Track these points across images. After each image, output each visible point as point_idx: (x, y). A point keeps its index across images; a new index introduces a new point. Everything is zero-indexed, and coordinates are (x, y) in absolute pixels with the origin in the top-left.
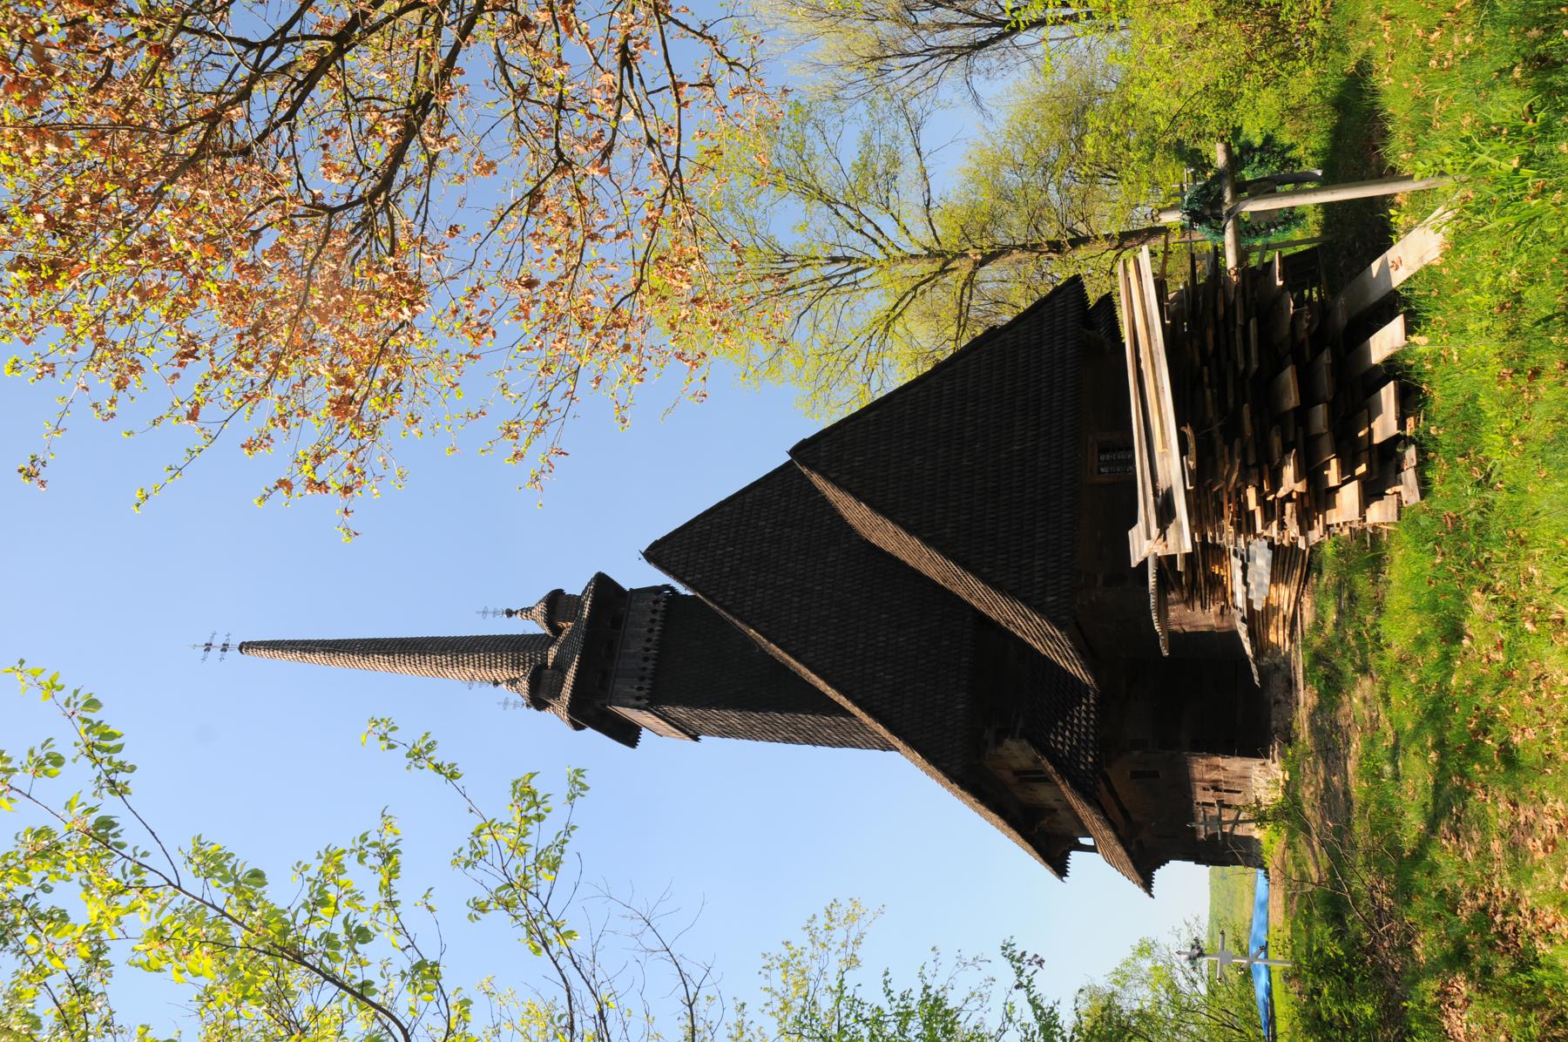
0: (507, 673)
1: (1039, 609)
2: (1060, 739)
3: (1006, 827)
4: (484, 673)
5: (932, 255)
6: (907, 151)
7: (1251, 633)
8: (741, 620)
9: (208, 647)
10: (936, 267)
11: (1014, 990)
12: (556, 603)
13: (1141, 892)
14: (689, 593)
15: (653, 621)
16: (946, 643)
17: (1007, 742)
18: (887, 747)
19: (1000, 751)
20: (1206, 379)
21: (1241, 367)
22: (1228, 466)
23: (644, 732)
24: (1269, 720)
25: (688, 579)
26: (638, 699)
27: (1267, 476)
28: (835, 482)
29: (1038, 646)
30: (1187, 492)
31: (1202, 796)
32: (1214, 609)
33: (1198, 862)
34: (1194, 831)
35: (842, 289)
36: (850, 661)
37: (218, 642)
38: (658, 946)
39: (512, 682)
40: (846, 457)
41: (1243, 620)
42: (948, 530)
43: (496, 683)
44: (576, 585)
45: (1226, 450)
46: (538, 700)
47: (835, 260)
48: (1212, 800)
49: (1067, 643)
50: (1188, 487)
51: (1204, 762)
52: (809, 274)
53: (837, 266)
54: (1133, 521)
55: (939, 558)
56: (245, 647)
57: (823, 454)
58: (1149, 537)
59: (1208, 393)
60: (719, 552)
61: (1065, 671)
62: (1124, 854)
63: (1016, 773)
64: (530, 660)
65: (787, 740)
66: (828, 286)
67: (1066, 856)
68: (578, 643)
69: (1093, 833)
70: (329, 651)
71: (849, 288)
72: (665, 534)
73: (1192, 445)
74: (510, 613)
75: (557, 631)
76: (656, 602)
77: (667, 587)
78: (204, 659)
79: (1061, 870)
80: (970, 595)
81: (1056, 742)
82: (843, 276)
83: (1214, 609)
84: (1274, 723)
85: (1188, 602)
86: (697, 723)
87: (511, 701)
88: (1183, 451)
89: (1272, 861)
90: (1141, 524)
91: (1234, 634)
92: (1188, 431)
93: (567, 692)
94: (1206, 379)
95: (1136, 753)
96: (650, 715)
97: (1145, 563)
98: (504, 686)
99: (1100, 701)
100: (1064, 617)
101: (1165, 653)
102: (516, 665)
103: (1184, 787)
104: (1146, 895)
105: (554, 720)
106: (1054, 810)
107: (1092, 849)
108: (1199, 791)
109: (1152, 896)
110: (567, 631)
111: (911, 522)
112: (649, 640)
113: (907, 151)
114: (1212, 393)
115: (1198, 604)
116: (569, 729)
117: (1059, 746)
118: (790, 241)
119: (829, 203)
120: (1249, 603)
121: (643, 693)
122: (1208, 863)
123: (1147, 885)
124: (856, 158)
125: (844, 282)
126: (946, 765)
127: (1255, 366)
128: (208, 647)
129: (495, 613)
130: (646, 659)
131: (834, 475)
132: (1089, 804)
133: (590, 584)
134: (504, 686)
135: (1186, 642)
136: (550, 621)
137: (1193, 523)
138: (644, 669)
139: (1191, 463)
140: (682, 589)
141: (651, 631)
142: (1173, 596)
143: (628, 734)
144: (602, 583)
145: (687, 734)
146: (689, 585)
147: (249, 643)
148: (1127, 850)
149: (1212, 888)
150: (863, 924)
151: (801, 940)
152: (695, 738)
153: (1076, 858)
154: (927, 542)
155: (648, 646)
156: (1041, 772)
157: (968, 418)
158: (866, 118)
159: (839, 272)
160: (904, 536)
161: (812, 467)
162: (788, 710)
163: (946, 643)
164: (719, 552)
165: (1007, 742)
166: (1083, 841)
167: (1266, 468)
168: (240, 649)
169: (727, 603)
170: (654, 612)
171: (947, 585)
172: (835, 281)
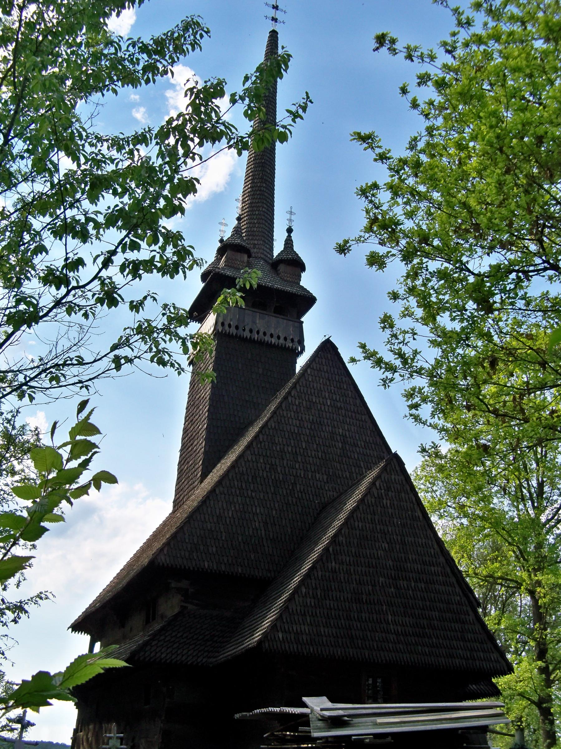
9: (276, 7)
14: (298, 369)
15: (279, 338)
16: (252, 556)
23: (200, 325)
25: (309, 371)
26: (223, 324)
37: (279, 15)
54: (332, 700)
57: (393, 477)
58: (322, 710)
67: (87, 632)
73: (378, 741)
74: (290, 230)
76: (292, 340)
77: (303, 349)
78: (267, 4)
79: (77, 627)
88: (376, 736)
90: (329, 705)
97: (305, 705)
101: (237, 716)
106: (123, 626)
111: (341, 538)
112: (265, 334)
121: (227, 327)
128: (276, 7)
129: (290, 220)
130: (251, 331)
131: (377, 484)
137: (330, 739)
138: (244, 330)
139: (367, 741)
140: (301, 362)
141: (272, 336)
153: (86, 638)
155: (261, 333)
156: (154, 619)
161: (384, 469)
163: (252, 556)
169: (290, 398)
170: (285, 339)
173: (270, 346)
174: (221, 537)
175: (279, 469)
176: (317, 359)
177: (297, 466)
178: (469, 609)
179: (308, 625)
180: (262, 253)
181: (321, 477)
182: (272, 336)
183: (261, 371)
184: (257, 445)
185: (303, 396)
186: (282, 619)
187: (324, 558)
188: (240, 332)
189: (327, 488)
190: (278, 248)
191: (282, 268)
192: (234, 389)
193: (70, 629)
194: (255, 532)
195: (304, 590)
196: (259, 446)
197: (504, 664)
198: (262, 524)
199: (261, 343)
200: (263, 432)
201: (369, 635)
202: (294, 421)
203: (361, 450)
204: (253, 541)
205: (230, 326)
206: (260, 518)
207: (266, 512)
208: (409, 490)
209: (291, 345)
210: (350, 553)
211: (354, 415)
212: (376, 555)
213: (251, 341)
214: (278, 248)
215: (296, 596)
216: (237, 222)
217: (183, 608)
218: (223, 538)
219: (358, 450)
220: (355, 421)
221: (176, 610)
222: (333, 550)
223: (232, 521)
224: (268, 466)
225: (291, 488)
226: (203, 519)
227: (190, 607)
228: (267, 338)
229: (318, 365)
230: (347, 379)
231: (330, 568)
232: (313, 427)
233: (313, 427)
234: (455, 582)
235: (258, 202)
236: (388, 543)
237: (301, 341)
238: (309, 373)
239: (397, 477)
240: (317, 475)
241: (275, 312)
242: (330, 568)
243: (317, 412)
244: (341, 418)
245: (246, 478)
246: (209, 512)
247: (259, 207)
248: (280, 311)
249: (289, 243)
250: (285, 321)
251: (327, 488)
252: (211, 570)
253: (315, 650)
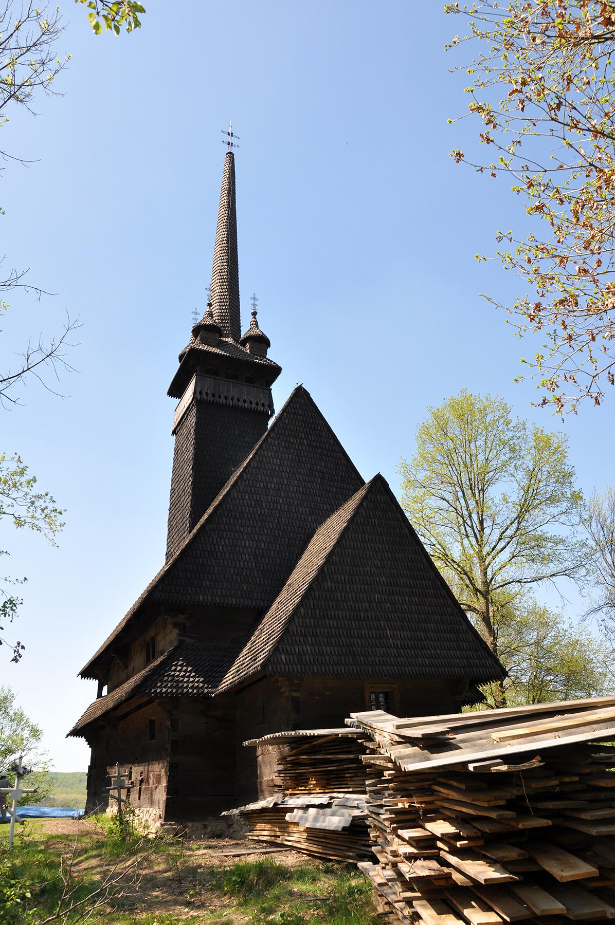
0: (216, 310)
1: (276, 650)
2: (179, 668)
3: (115, 633)
4: (215, 301)
5: (487, 584)
6: (553, 567)
7: (264, 810)
8: (259, 449)
10: (480, 586)
12: (261, 342)
13: (70, 728)
14: (269, 427)
15: (251, 403)
16: (245, 588)
17: (176, 631)
18: (168, 556)
19: (170, 626)
20: (567, 780)
21: (584, 816)
22: (485, 805)
23: (178, 400)
24: (193, 821)
25: (285, 414)
26: (201, 393)
27: (472, 844)
28: (360, 505)
29: (245, 651)
30: (465, 764)
31: (137, 771)
32: (278, 781)
33: (90, 768)
34: (112, 765)
35: (462, 527)
36: (232, 521)
38: (33, 361)
39: (211, 315)
40: (377, 512)
41: (276, 804)
42: (329, 584)
43: (210, 305)
44: (272, 355)
45: (502, 803)
46: (198, 330)
47: (481, 522)
48: (133, 778)
49: (251, 670)
50: (471, 767)
51: (163, 773)
52: (472, 504)
53: (478, 525)
55: (309, 579)
56: (231, 156)
57: (379, 497)
59: (555, 783)
60: (303, 435)
61: (226, 672)
62: (96, 716)
63: (153, 640)
64: (224, 327)
65: (173, 491)
66: (464, 519)
67: (95, 677)
68: (236, 355)
69: (110, 695)
70: (229, 205)
71: (463, 531)
74: (254, 314)
75: (243, 343)
76: (263, 405)
77: (273, 412)
78: (223, 131)
79: (86, 673)
80: (280, 603)
81: (176, 665)
82: (472, 527)
83: (278, 781)
84: (190, 824)
85: (283, 760)
86: (184, 432)
87: (198, 317)
88: (507, 759)
89: (89, 824)
92: (535, 763)
93: (205, 348)
94: (567, 780)
95: (168, 723)
96: (190, 400)
98: (208, 310)
99: (206, 697)
100: (270, 668)
101: (246, 743)
102: (222, 318)
103: (142, 757)
104: (68, 732)
105: (185, 341)
106: (126, 668)
107: (100, 695)
108: (141, 769)
109: (67, 736)
110: (243, 349)
111: (334, 558)
112: (238, 400)
113: (553, 567)
114: (553, 787)
115: (281, 767)
116: (180, 352)
117: (174, 668)
118: (494, 493)
119: (518, 517)
120: (291, 810)
121: (204, 396)
122: (90, 775)
123: (75, 733)
125: (468, 529)
126: (160, 587)
127: (594, 831)
129: (254, 305)
130: (226, 398)
131: (365, 504)
132: (133, 690)
133: (274, 363)
134: (208, 310)
135: (250, 760)
136: (249, 339)
138: (220, 397)
140: (271, 422)
141: (245, 401)
142: (286, 749)
143: (176, 390)
144: (275, 371)
146: (275, 425)
147: (233, 158)
148: (99, 718)
149: (74, 774)
150: (47, 531)
151: (37, 489)
152: (174, 432)
153: (94, 684)
154: (321, 570)
155: (235, 400)
157: (407, 599)
158: (574, 540)
159: (474, 525)
160: (324, 554)
162: (193, 489)
163: (245, 588)
164: (303, 435)
165: (176, 631)
166: (105, 689)
167: (481, 843)
168: (230, 153)
170: (257, 404)
171: (286, 587)
172: (469, 522)
173: (243, 410)
174: (214, 571)
175: (264, 505)
176: (292, 404)
177: (281, 501)
178: (461, 619)
179: (310, 645)
182: (245, 401)
183: (237, 432)
185: (282, 437)
186: (284, 641)
187: (320, 579)
188: (217, 398)
189: (310, 520)
192: (214, 449)
193: (80, 676)
194: (246, 564)
195: (302, 611)
196: (244, 484)
197: (499, 669)
198: (252, 557)
199: (235, 408)
200: (247, 472)
201: (370, 650)
202: (275, 460)
203: (338, 484)
204: (244, 573)
206: (249, 551)
207: (255, 545)
208: (394, 509)
209: (262, 409)
210: (344, 571)
212: (369, 572)
213: (227, 406)
215: (296, 618)
217: (181, 642)
218: (216, 571)
219: (335, 484)
220: (330, 459)
221: (175, 644)
224: (253, 503)
225: (276, 521)
226: (195, 555)
227: (188, 640)
229: (293, 409)
230: (320, 421)
231: (326, 587)
232: (292, 464)
233: (292, 464)
234: (446, 594)
236: (380, 561)
237: (271, 405)
238: (285, 416)
240: (300, 509)
241: (246, 382)
242: (326, 587)
243: (295, 451)
244: (318, 456)
245: (233, 515)
248: (250, 381)
251: (310, 520)
252: (206, 603)
253: (319, 670)
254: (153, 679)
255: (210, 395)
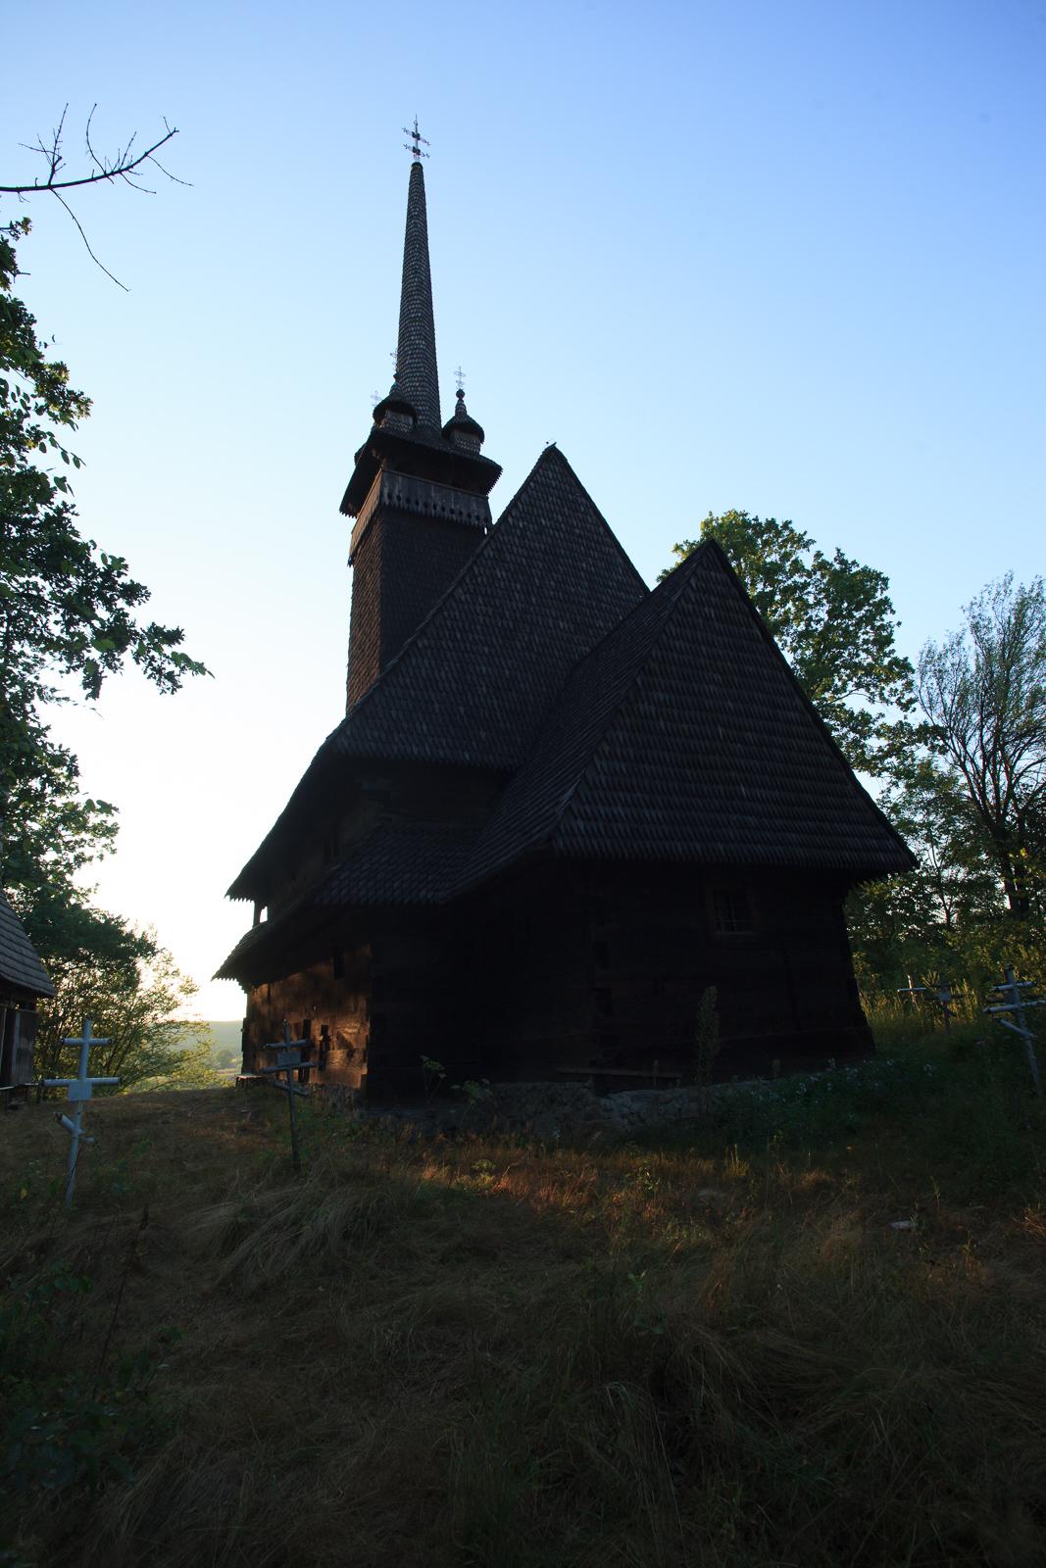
9: (416, 136)
11: (101, 553)
15: (461, 513)
37: (421, 146)
56: (417, 171)
67: (249, 897)
72: (584, 484)
76: (478, 518)
91: (739, 1159)
105: (361, 429)
109: (213, 978)
112: (443, 509)
121: (395, 500)
124: (178, 1020)
128: (416, 136)
138: (417, 503)
141: (452, 512)
145: (358, 547)
153: (249, 906)
155: (438, 508)
180: (428, 420)
181: (566, 627)
184: (471, 580)
188: (413, 506)
190: (447, 414)
191: (456, 435)
193: (228, 897)
205: (399, 498)
211: (598, 546)
214: (447, 414)
216: (394, 380)
222: (643, 682)
223: (449, 675)
228: (447, 514)
230: (584, 500)
235: (419, 363)
239: (718, 576)
246: (411, 673)
247: (420, 367)
249: (460, 408)
250: (466, 496)
254: (342, 877)
255: (403, 501)
